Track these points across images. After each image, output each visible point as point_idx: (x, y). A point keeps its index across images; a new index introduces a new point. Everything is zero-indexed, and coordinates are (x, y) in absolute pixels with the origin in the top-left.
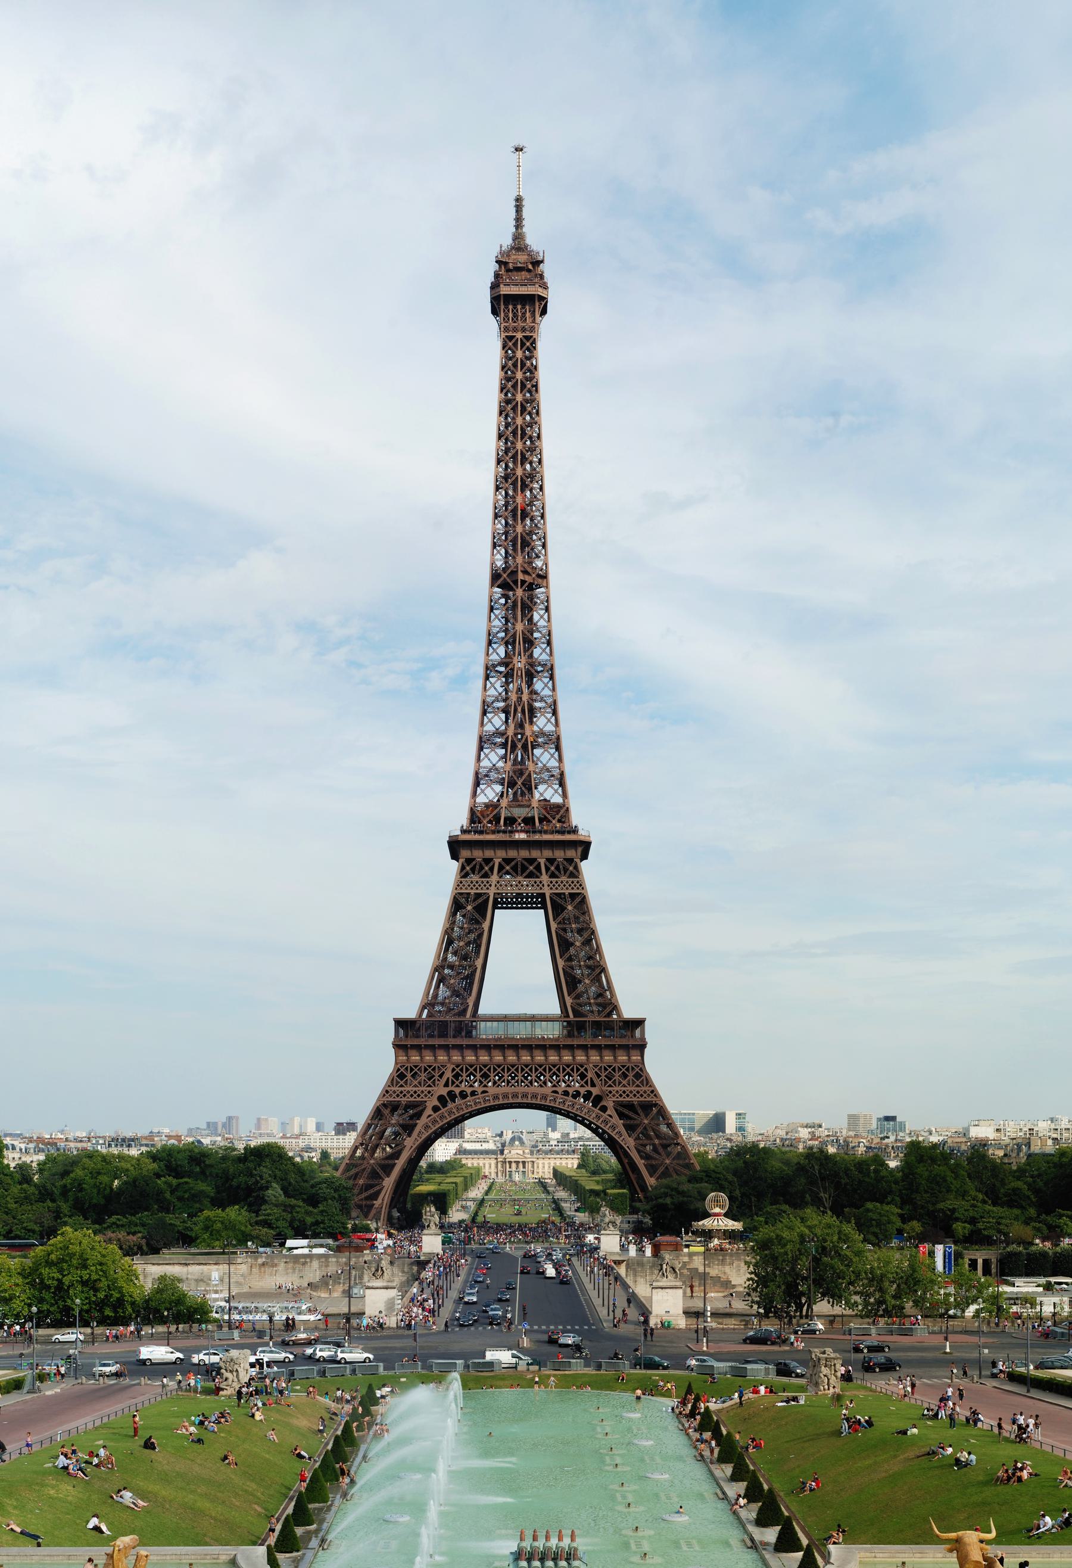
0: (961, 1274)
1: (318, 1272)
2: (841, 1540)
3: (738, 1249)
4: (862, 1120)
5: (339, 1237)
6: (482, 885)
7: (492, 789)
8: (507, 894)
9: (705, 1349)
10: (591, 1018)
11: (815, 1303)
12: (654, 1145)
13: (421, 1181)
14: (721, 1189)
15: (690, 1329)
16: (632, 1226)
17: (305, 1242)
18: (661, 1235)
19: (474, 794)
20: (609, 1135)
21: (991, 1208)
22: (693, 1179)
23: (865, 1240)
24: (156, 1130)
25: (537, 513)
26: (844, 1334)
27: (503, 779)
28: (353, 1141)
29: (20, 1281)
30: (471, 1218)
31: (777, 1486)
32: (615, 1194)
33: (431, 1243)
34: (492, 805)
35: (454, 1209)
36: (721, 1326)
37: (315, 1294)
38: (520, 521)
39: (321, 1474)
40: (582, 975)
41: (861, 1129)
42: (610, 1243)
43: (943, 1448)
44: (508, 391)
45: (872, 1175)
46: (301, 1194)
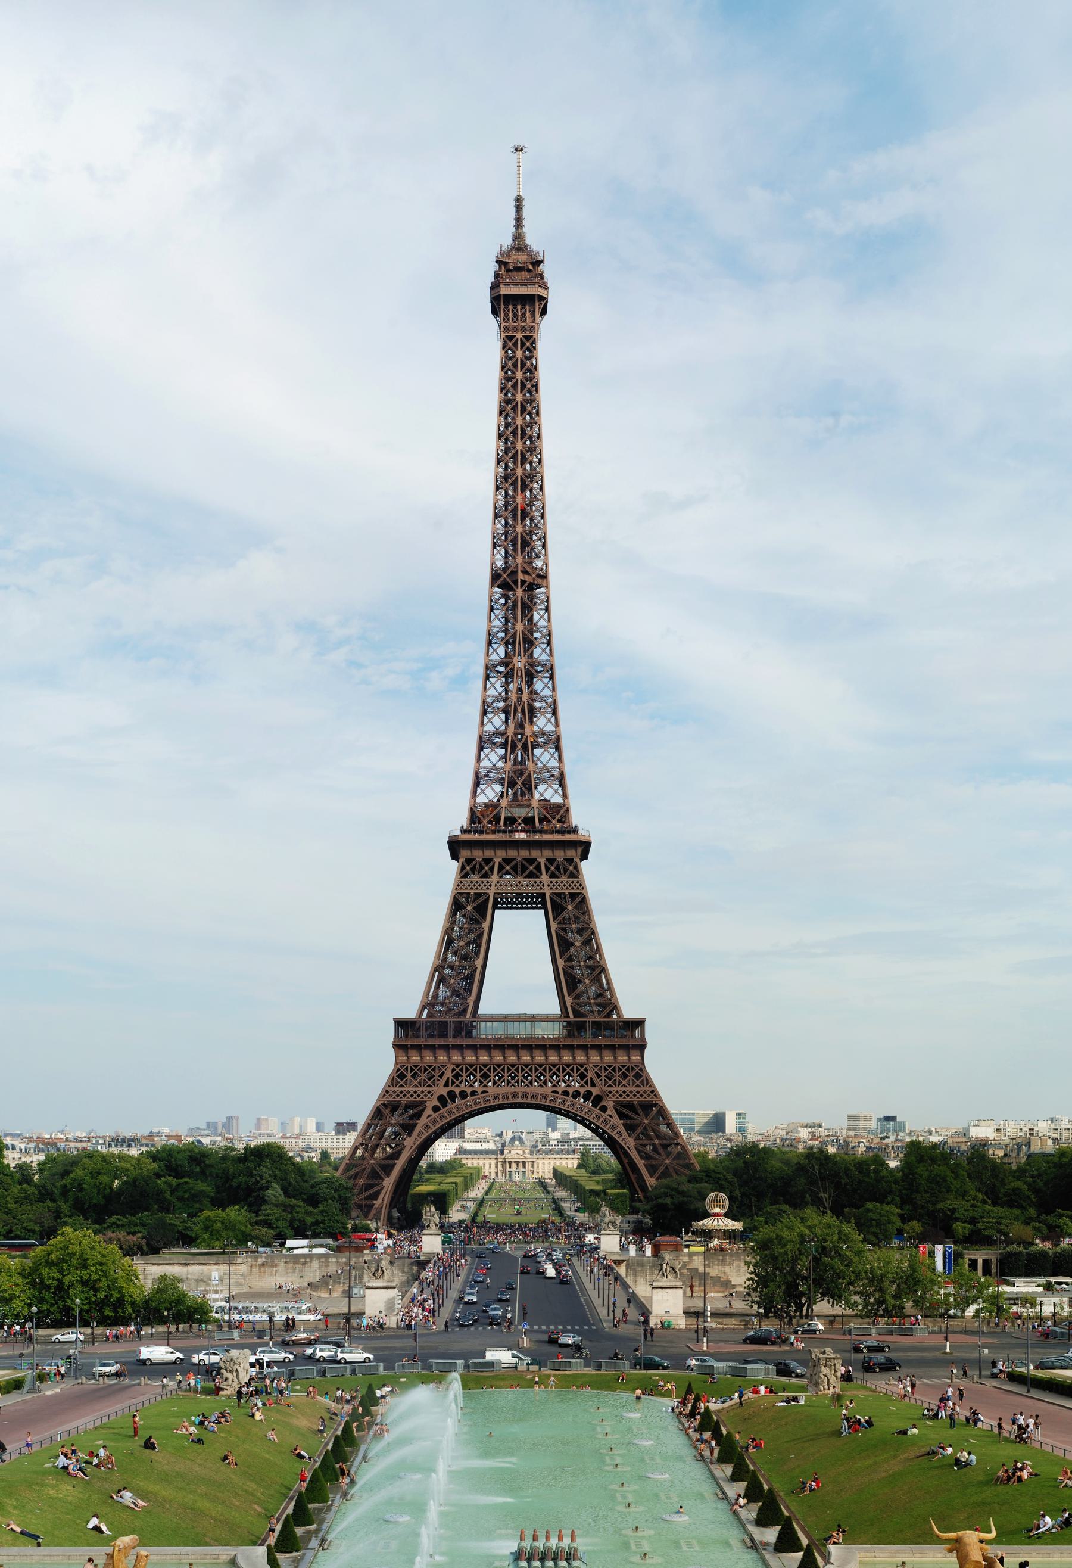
0: (961, 1274)
1: (318, 1272)
2: (841, 1540)
3: (738, 1249)
4: (862, 1120)
5: (339, 1237)
6: (482, 885)
7: (492, 789)
8: (507, 894)
9: (705, 1349)
10: (591, 1018)
11: (815, 1303)
12: (654, 1145)
13: (421, 1181)
14: (721, 1189)
15: (690, 1329)
16: (632, 1226)
17: (305, 1242)
18: (661, 1235)
19: (474, 794)
20: (609, 1135)
21: (991, 1208)
22: (693, 1179)
23: (865, 1240)
24: (156, 1130)
25: (537, 513)
26: (844, 1334)
27: (503, 779)
28: (353, 1141)
29: (20, 1281)
30: (471, 1218)
31: (777, 1486)
32: (615, 1194)
33: (431, 1243)
34: (492, 805)
35: (454, 1209)
36: (721, 1326)
37: (315, 1294)
38: (520, 521)
39: (321, 1474)
40: (582, 975)
41: (861, 1129)
42: (610, 1243)
43: (943, 1448)
44: (508, 391)
45: (872, 1175)
46: (301, 1194)
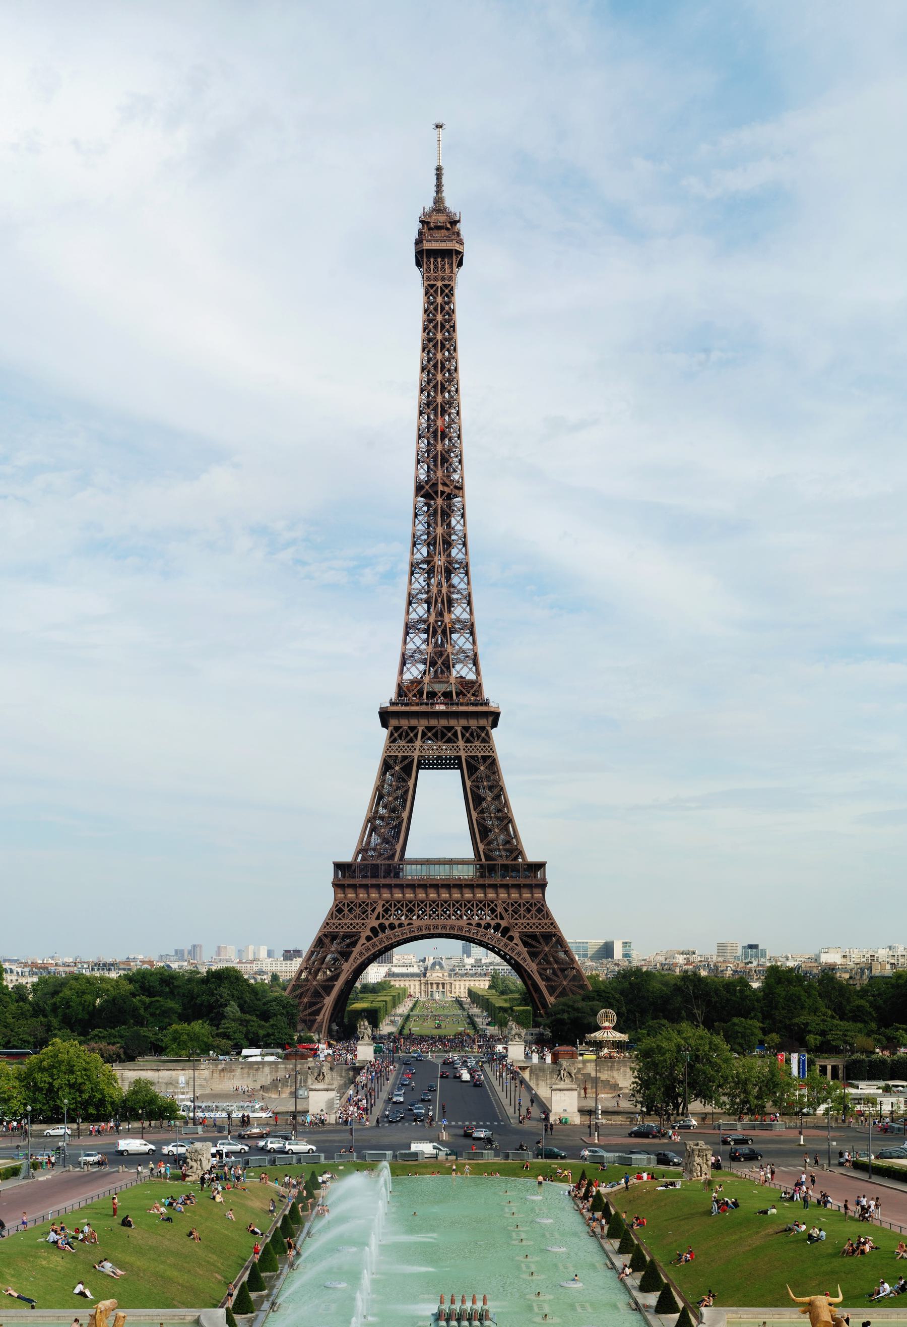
1: (269, 1077)
2: (711, 1304)
3: (625, 1057)
4: (729, 948)
5: (287, 1047)
6: (408, 749)
7: (416, 667)
8: (429, 756)
9: (596, 1141)
10: (500, 862)
11: (690, 1103)
12: (553, 969)
13: (356, 999)
14: (610, 1006)
15: (584, 1125)
16: (534, 1037)
17: (258, 1051)
18: (559, 1045)
19: (401, 672)
20: (515, 960)
22: (586, 998)
23: (732, 1050)
25: (455, 435)
27: (426, 659)
28: (298, 966)
30: (398, 1031)
31: (657, 1258)
32: (520, 1011)
33: (365, 1052)
34: (416, 682)
37: (266, 1095)
38: (440, 441)
39: (271, 1247)
40: (493, 825)
41: (729, 956)
44: (430, 331)
45: (738, 994)
46: (255, 1010)
